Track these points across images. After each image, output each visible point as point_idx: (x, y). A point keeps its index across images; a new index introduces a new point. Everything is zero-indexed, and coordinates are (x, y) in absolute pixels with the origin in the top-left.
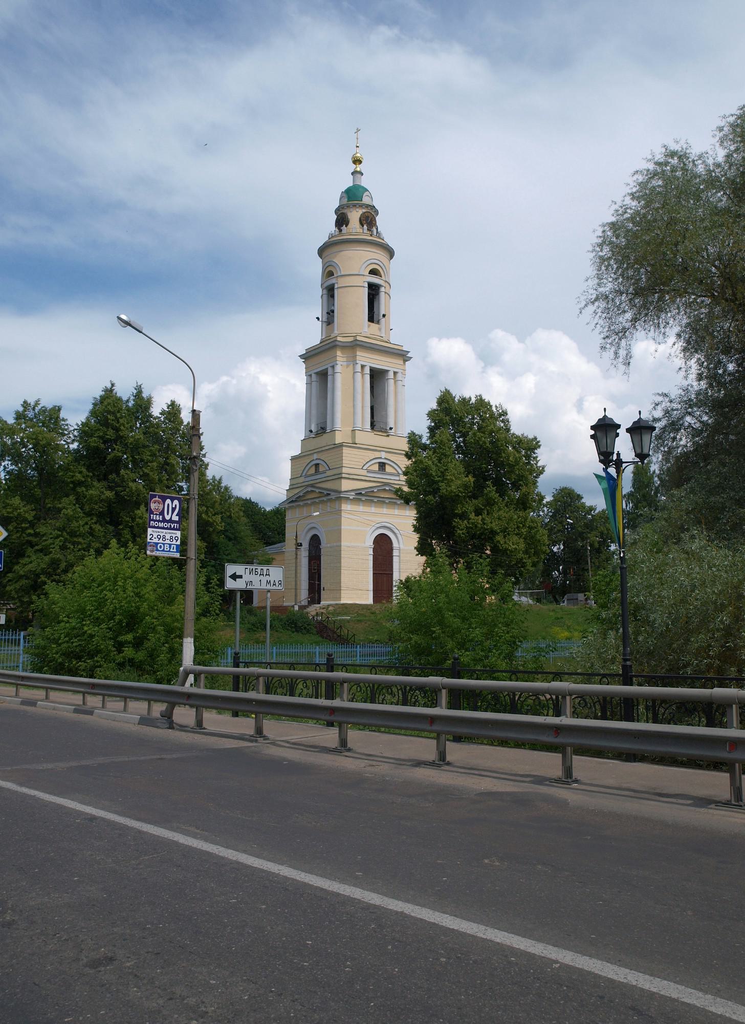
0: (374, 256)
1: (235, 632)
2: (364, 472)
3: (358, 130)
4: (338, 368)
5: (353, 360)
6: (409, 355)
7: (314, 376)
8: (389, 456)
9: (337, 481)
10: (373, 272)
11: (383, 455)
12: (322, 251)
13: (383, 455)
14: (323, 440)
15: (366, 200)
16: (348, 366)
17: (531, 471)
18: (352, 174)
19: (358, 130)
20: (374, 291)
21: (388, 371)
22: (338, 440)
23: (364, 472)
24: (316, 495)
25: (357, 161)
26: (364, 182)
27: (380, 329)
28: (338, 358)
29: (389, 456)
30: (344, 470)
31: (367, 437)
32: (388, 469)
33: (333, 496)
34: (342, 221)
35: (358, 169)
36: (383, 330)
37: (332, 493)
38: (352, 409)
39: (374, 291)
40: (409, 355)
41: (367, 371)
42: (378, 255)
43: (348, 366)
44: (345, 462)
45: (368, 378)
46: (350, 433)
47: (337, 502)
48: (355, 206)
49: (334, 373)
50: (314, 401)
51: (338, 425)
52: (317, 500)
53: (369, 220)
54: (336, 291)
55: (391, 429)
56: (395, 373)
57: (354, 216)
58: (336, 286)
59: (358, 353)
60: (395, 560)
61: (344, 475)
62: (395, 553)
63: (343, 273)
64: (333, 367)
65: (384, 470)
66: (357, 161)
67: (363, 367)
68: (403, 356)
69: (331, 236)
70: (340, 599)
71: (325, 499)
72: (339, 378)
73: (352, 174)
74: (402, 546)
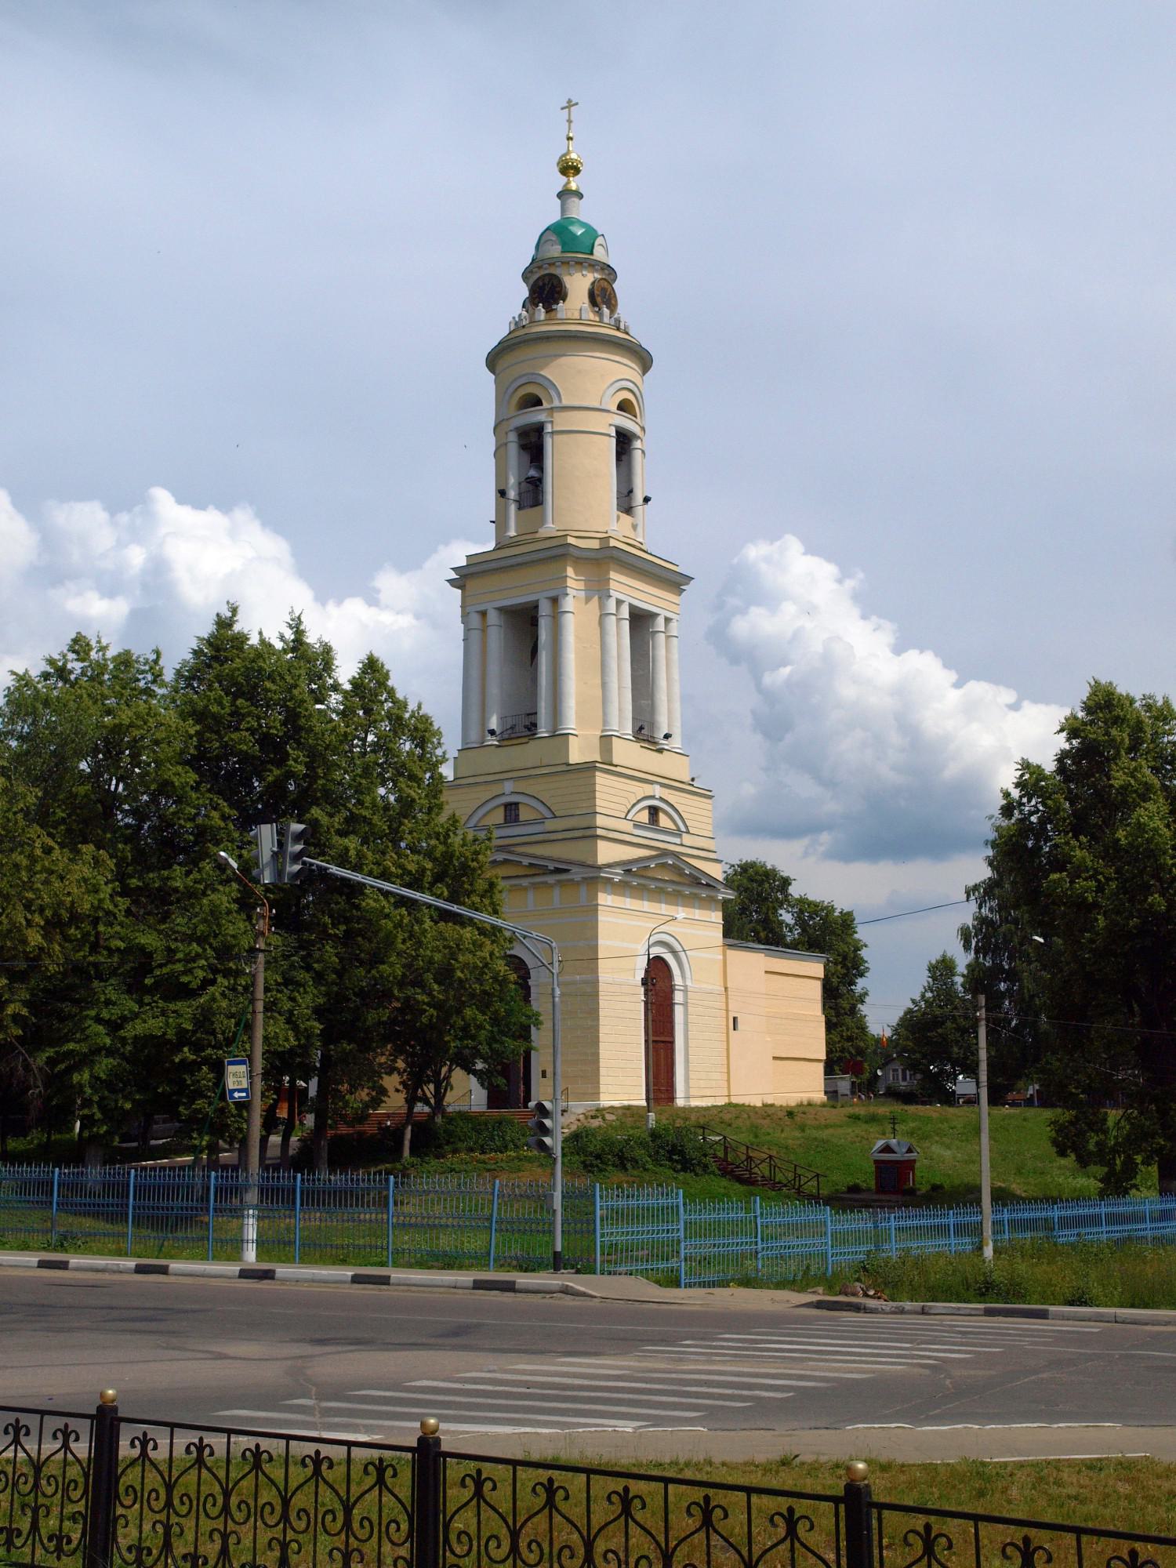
0: (615, 370)
1: (553, 1174)
2: (628, 826)
3: (570, 105)
4: (569, 604)
5: (599, 589)
6: (454, 576)
7: (493, 617)
8: (521, 786)
9: (581, 844)
10: (624, 407)
11: (658, 791)
12: (493, 361)
13: (658, 791)
14: (526, 754)
15: (599, 254)
16: (588, 600)
17: (1001, 837)
18: (560, 195)
19: (570, 105)
20: (624, 441)
21: (658, 615)
22: (575, 757)
23: (628, 826)
24: (521, 872)
25: (569, 168)
26: (582, 211)
27: (635, 527)
28: (570, 583)
29: (521, 786)
30: (600, 821)
31: (628, 753)
32: (524, 814)
33: (577, 874)
34: (545, 290)
35: (573, 186)
36: (640, 529)
37: (574, 869)
38: (599, 692)
39: (624, 441)
40: (454, 576)
41: (625, 612)
42: (622, 369)
43: (588, 600)
44: (601, 804)
45: (626, 625)
46: (597, 741)
47: (583, 890)
48: (580, 263)
49: (557, 615)
50: (494, 669)
51: (571, 722)
52: (525, 882)
53: (602, 297)
54: (548, 442)
55: (667, 736)
56: (667, 620)
57: (579, 284)
58: (548, 428)
59: (613, 575)
60: (678, 1011)
61: (599, 832)
62: (678, 997)
63: (565, 402)
64: (555, 601)
65: (516, 819)
66: (569, 168)
67: (619, 602)
68: (674, 582)
69: (518, 325)
70: (596, 1095)
71: (551, 879)
72: (572, 626)
73: (560, 195)
74: (689, 983)
